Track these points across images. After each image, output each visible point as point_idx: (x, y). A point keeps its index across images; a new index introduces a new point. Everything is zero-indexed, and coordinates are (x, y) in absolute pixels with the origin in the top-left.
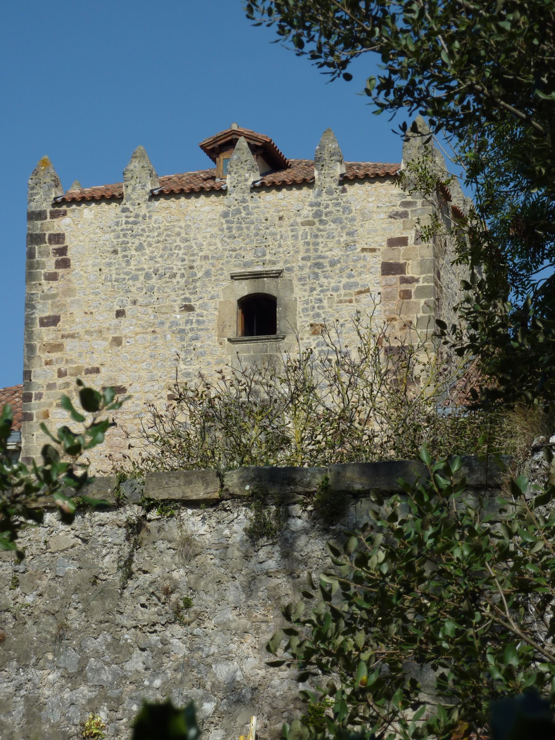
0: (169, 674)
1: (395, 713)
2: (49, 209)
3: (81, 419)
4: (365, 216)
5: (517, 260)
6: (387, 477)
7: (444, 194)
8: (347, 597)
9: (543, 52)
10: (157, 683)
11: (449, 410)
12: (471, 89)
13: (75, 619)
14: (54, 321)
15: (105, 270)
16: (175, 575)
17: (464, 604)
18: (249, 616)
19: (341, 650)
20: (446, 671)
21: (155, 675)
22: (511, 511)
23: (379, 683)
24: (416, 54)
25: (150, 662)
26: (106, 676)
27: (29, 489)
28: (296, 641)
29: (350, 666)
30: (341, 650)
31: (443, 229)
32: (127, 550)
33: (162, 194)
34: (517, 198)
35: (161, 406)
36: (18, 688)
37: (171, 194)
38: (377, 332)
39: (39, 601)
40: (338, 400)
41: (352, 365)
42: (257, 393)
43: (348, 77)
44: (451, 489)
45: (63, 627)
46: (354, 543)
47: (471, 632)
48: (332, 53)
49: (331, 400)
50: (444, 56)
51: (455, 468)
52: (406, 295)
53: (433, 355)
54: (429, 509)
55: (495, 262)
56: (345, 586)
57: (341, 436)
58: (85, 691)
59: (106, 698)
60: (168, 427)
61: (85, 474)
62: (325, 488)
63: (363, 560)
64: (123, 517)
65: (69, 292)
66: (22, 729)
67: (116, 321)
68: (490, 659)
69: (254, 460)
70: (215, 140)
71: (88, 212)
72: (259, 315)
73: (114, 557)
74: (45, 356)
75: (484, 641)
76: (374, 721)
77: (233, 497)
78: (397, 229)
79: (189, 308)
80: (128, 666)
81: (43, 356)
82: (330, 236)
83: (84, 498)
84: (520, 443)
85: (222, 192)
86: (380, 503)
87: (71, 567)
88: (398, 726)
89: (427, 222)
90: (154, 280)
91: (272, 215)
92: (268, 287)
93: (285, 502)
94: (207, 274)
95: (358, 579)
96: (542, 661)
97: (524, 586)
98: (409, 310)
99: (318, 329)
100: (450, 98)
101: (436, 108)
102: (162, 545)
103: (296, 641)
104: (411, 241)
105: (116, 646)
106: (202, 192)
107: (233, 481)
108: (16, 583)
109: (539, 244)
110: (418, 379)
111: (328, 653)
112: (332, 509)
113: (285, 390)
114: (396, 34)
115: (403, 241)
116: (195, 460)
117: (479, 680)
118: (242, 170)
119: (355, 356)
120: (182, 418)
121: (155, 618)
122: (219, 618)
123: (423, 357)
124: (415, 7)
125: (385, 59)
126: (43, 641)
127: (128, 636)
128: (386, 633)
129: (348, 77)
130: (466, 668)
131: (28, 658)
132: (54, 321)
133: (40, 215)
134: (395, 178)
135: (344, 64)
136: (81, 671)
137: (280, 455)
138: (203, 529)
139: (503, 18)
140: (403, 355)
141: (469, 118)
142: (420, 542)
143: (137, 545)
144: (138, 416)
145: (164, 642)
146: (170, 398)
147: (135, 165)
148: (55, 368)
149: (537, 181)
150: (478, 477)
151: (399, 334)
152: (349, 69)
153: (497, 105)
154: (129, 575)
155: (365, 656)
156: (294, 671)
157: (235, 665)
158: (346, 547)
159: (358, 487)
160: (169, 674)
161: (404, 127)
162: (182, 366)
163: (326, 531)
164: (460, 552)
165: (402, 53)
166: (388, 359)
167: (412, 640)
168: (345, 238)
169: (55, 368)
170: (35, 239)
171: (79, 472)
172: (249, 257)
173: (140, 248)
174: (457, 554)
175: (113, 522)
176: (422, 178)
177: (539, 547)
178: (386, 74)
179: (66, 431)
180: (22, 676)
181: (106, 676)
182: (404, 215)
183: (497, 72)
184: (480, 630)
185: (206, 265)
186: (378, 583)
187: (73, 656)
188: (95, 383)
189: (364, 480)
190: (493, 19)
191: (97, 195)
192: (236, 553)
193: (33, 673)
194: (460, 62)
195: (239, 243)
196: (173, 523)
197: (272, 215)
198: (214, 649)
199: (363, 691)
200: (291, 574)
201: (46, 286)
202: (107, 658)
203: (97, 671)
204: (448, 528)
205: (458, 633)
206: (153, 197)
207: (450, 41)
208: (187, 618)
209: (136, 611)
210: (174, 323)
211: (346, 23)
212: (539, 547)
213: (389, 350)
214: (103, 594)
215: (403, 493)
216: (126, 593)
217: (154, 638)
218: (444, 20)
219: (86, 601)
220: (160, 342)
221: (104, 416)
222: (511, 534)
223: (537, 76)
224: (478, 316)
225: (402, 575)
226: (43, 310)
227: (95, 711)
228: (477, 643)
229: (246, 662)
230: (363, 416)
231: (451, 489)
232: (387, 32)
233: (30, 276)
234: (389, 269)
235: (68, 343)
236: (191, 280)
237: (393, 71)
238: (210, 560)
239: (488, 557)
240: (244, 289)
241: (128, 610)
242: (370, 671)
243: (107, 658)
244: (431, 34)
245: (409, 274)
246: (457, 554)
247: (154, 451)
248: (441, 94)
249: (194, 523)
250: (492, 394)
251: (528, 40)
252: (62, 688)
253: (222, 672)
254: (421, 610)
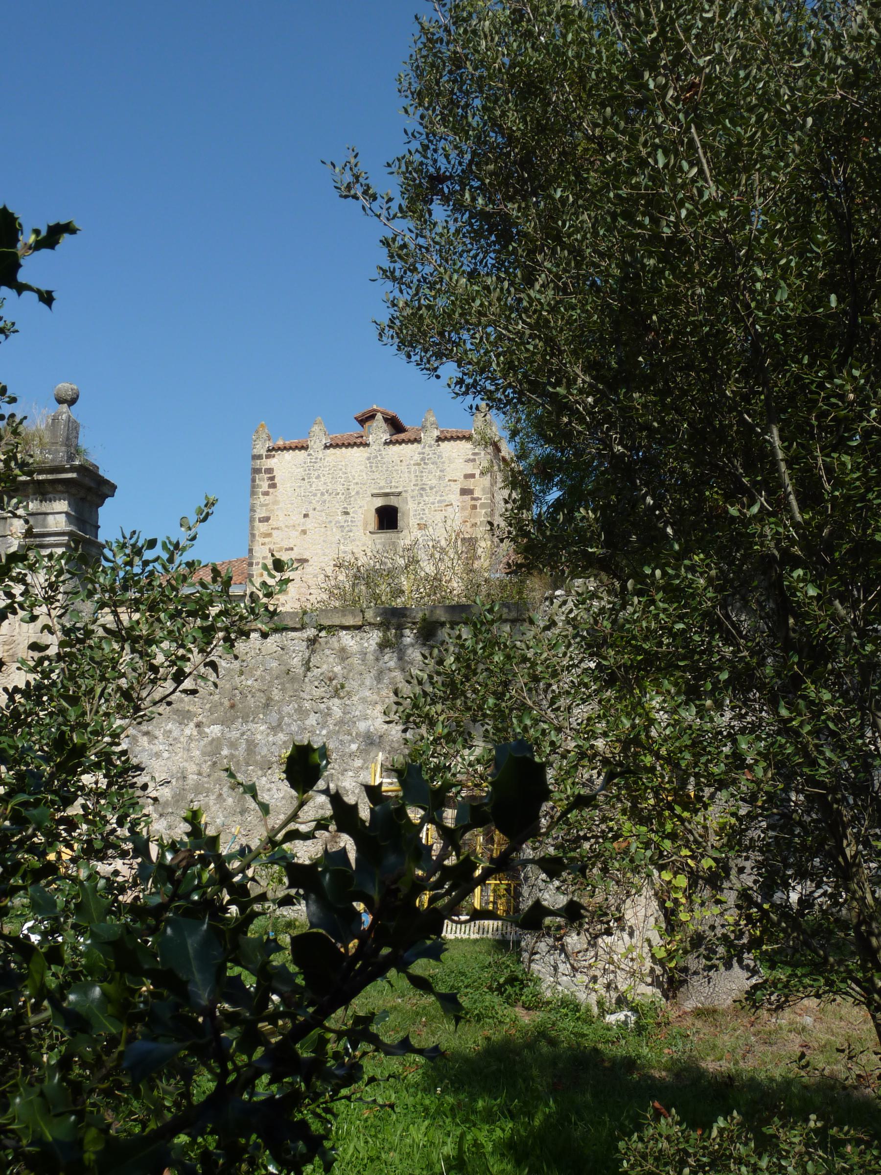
0: (331, 727)
1: (458, 752)
2: (265, 453)
3: (274, 577)
4: (451, 461)
5: (538, 488)
6: (460, 613)
7: (497, 449)
8: (432, 684)
9: (552, 364)
10: (324, 732)
11: (498, 575)
12: (510, 385)
13: (276, 694)
14: (266, 519)
15: (298, 490)
16: (335, 669)
17: (500, 688)
18: (378, 693)
19: (427, 714)
20: (489, 728)
21: (323, 728)
22: (530, 635)
23: (449, 734)
24: (478, 363)
25: (320, 720)
26: (294, 728)
27: (242, 618)
28: (401, 709)
29: (432, 724)
30: (427, 714)
31: (496, 468)
32: (307, 655)
33: (331, 446)
34: (539, 450)
35: (329, 570)
36: (243, 734)
37: (337, 446)
38: (457, 529)
39: (255, 683)
40: (433, 568)
41: (442, 548)
42: (386, 564)
43: (438, 377)
44: (493, 622)
45: (269, 699)
46: (436, 651)
47: (504, 704)
48: (428, 362)
49: (429, 568)
50: (494, 366)
51: (496, 609)
52: (474, 507)
53: (489, 543)
54: (481, 632)
55: (525, 489)
56: (430, 677)
57: (434, 589)
60: (333, 583)
61: (275, 610)
62: (424, 620)
63: (440, 662)
64: (305, 635)
65: (276, 502)
66: (244, 759)
67: (303, 520)
68: (514, 720)
69: (383, 603)
70: (363, 415)
71: (288, 455)
72: (388, 518)
73: (300, 658)
74: (261, 540)
75: (511, 710)
76: (446, 755)
77: (370, 624)
78: (469, 469)
79: (347, 513)
80: (307, 722)
81: (260, 540)
82: (430, 472)
83: (278, 625)
84: (537, 595)
85: (367, 445)
86: (452, 628)
87: (274, 664)
88: (460, 760)
89: (486, 464)
90: (326, 496)
91: (397, 459)
92: (393, 501)
93: (400, 628)
94: (358, 493)
95: (439, 674)
96: (544, 722)
97: (536, 679)
98: (475, 516)
99: (422, 527)
100: (497, 390)
101: (490, 396)
102: (327, 652)
103: (401, 709)
104: (477, 476)
105: (300, 710)
106: (355, 444)
107: (370, 615)
108: (242, 673)
109: (551, 479)
110: (480, 557)
111: (420, 716)
112: (428, 632)
113: (402, 562)
114: (466, 352)
115: (473, 476)
116: (350, 604)
117: (508, 733)
118: (379, 432)
119: (443, 543)
120: (342, 577)
121: (323, 695)
122: (361, 695)
123: (483, 544)
124: (477, 335)
125: (459, 366)
126: (257, 707)
127: (307, 705)
128: (454, 705)
129: (438, 377)
130: (500, 726)
131: (248, 717)
132: (266, 519)
133: (259, 457)
134: (468, 438)
135: (435, 369)
136: (279, 725)
137: (399, 600)
138: (352, 643)
139: (528, 343)
140: (471, 543)
141: (509, 402)
142: (475, 652)
143: (313, 651)
144: (316, 576)
145: (328, 708)
146: (335, 566)
147: (316, 428)
148: (267, 547)
149: (548, 440)
150: (513, 615)
151: (469, 530)
152: (438, 373)
153: (525, 395)
154: (309, 669)
155: (441, 718)
156: (401, 727)
157: (370, 722)
158: (431, 654)
159: (443, 619)
160: (331, 727)
161: (471, 408)
162: (342, 547)
163: (424, 645)
164: (498, 658)
165: (469, 363)
166: (463, 544)
167: (469, 709)
168: (438, 473)
169: (267, 547)
170: (257, 471)
171: (271, 608)
172: (382, 483)
173: (318, 477)
174: (496, 659)
175: (299, 638)
176: (483, 438)
177: (545, 655)
178: (460, 375)
179: (264, 584)
180: (245, 728)
181: (294, 728)
182: (474, 460)
183: (525, 375)
184: (509, 703)
185: (357, 488)
186: (450, 675)
187: (275, 716)
188: (284, 557)
189: (447, 615)
190: (523, 343)
191: (293, 446)
192: (371, 657)
193: (251, 726)
194: (503, 369)
195: (376, 475)
196: (335, 639)
197: (397, 459)
198: (357, 713)
199: (439, 738)
200: (403, 670)
201: (262, 499)
202: (295, 717)
203: (289, 725)
204: (493, 643)
205: (496, 705)
206: (326, 447)
207: (498, 356)
208: (342, 695)
209: (312, 690)
210: (337, 522)
211: (437, 344)
212: (545, 655)
213: (463, 539)
214: (293, 680)
215: (466, 623)
216: (307, 680)
217: (323, 706)
218: (494, 344)
219: (283, 684)
220: (329, 533)
221: (287, 575)
222: (528, 648)
223: (549, 378)
224: (514, 520)
225: (463, 670)
226: (260, 513)
228: (507, 711)
229: (375, 722)
230: (448, 578)
231: (493, 622)
232: (461, 350)
233: (253, 493)
234: (464, 492)
235: (275, 533)
236: (348, 497)
237: (464, 374)
238: (356, 661)
239: (515, 661)
240: (379, 502)
241: (307, 689)
242: (444, 727)
243: (295, 717)
244: (487, 352)
246: (496, 659)
247: (325, 597)
248: (493, 388)
249: (347, 639)
250: (519, 566)
251: (543, 356)
252: (268, 735)
253: (362, 726)
254: (476, 691)
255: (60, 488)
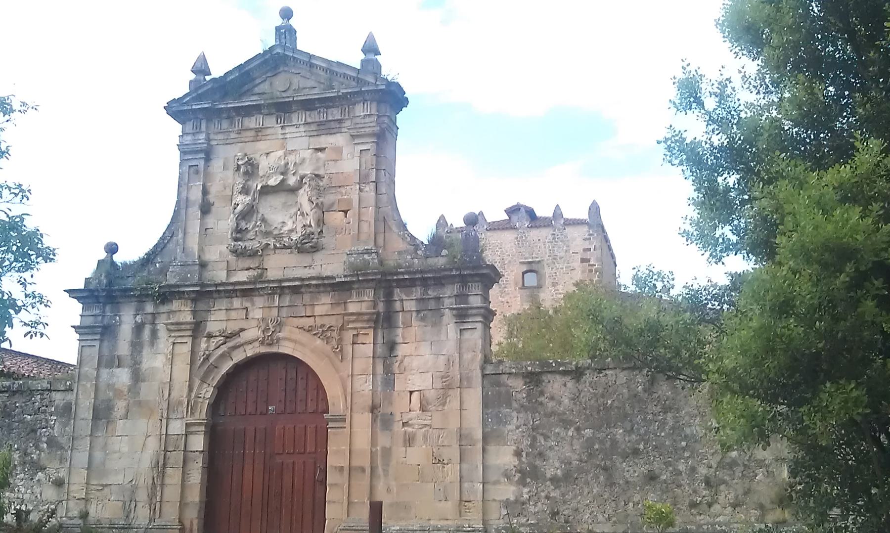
4: (574, 239)
21: (662, 431)
26: (642, 431)
58: (634, 437)
59: (643, 440)
78: (587, 245)
91: (536, 239)
94: (510, 262)
104: (592, 250)
185: (509, 258)
195: (522, 250)
197: (536, 239)
227: (639, 444)
245: (592, 263)
255: (477, 279)
